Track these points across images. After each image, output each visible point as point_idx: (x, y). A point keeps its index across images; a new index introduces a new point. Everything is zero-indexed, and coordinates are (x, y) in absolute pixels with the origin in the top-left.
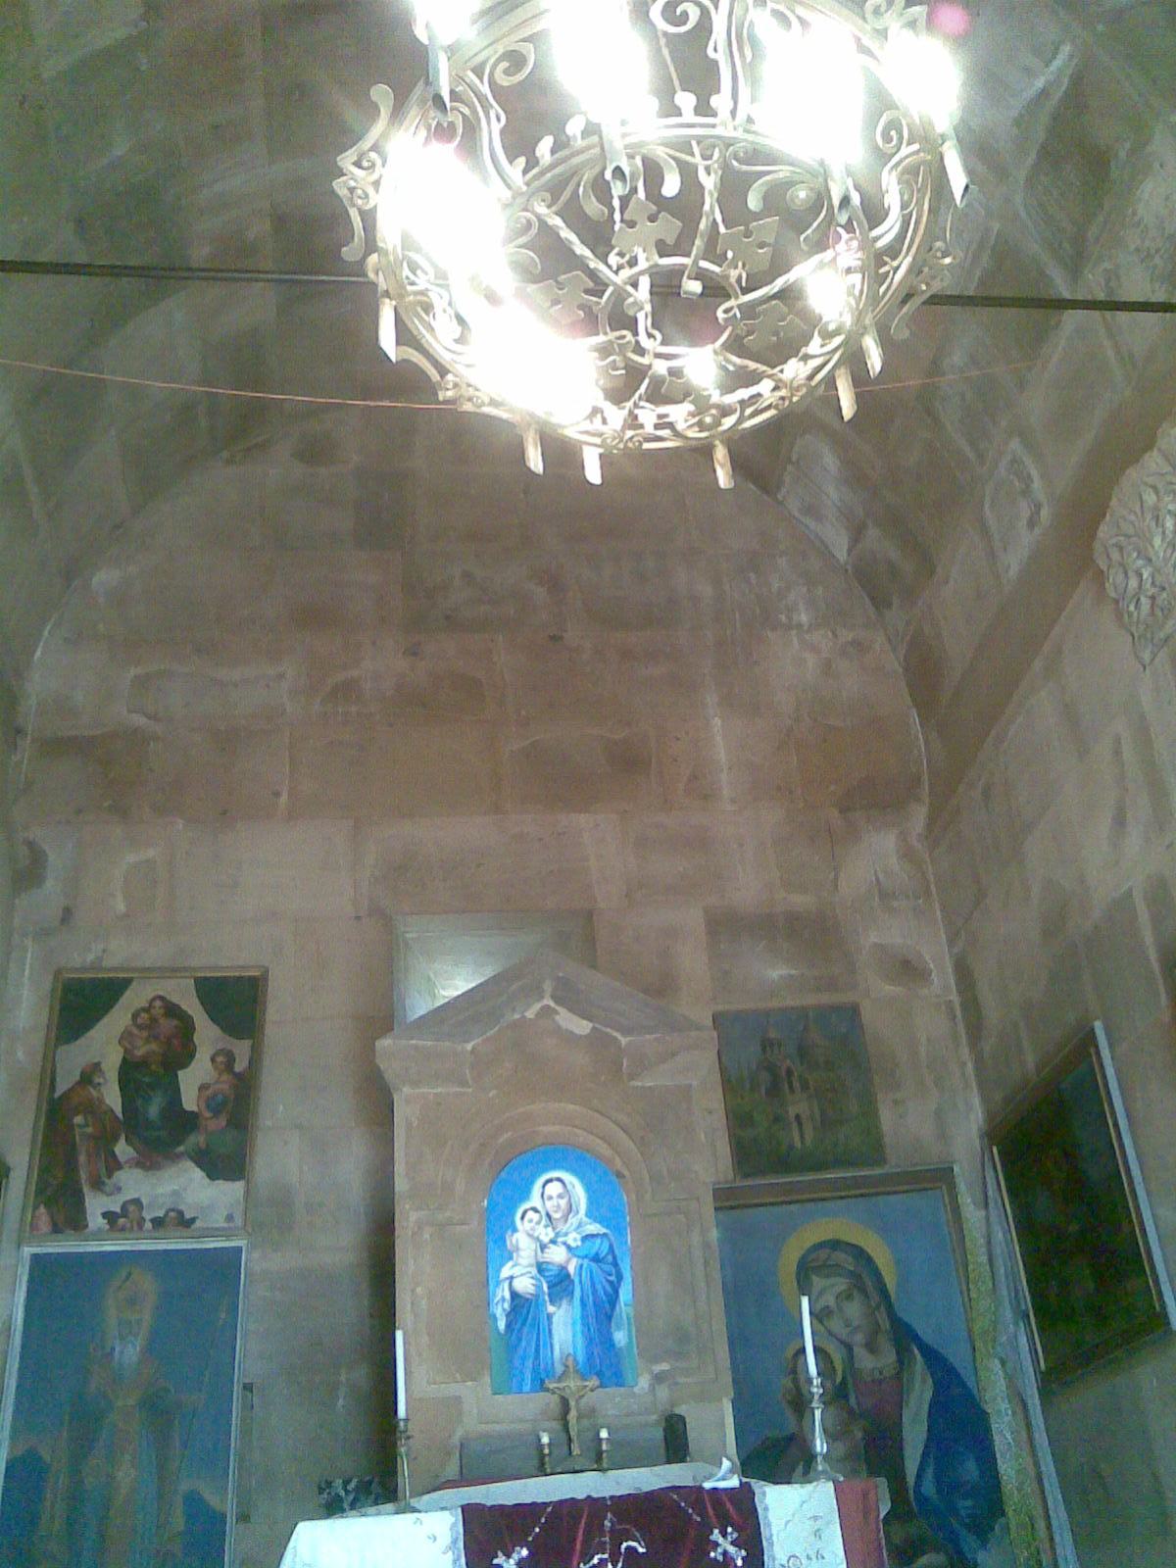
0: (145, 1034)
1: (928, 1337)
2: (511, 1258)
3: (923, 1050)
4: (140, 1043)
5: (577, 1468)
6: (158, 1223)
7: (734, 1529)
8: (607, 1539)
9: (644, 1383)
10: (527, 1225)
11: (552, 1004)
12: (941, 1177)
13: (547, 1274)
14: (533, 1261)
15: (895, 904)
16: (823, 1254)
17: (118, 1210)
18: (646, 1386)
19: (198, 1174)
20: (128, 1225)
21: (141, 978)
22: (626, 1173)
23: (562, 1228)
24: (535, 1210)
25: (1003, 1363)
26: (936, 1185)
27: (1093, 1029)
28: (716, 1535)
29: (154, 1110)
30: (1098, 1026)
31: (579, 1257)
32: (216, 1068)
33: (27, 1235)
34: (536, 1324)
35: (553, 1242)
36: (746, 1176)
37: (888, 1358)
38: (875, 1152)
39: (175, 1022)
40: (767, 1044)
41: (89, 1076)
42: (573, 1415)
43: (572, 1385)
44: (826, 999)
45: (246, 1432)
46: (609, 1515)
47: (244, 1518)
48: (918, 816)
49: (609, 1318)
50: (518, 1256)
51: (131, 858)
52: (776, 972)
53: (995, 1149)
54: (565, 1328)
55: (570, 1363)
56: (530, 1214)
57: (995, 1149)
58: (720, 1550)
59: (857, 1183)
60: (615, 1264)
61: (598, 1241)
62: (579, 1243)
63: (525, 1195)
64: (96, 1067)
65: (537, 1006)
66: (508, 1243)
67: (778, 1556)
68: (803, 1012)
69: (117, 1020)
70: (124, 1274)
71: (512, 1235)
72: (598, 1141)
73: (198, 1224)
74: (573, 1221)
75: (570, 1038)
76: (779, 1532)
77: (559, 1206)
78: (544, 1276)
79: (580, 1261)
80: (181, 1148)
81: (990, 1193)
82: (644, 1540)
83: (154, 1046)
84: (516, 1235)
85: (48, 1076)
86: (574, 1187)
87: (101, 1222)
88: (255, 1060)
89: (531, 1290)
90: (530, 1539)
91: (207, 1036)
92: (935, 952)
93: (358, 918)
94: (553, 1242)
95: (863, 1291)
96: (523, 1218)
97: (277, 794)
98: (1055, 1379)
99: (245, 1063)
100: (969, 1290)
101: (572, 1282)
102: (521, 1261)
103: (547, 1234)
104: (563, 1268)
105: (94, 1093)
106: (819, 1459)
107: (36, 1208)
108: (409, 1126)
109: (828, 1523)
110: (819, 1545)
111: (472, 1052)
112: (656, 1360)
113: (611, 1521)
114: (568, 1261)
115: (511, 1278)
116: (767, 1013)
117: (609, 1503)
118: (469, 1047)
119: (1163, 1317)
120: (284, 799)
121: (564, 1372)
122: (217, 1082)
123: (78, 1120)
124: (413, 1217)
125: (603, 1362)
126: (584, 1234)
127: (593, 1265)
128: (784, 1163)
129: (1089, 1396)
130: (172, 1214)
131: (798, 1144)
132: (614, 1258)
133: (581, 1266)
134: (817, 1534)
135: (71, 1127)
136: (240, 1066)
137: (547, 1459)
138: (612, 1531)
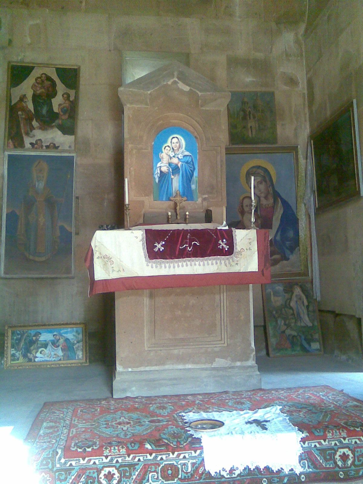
0: (40, 86)
1: (283, 196)
2: (161, 161)
3: (293, 109)
4: (38, 89)
5: (179, 222)
6: (47, 147)
7: (226, 241)
8: (188, 241)
9: (200, 200)
10: (166, 151)
11: (177, 80)
12: (294, 149)
13: (172, 166)
14: (167, 162)
15: (290, 58)
16: (254, 170)
17: (35, 143)
18: (200, 201)
19: (59, 133)
20: (38, 147)
21: (38, 66)
22: (198, 137)
23: (177, 152)
24: (169, 146)
25: (305, 205)
26: (291, 151)
27: (352, 102)
28: (220, 242)
29: (44, 111)
30: (355, 101)
31: (181, 162)
32: (64, 99)
33: (6, 148)
34: (168, 180)
35: (174, 157)
36: (233, 144)
37: (271, 201)
38: (274, 140)
39: (49, 83)
40: (243, 103)
41: (23, 98)
42: (178, 208)
43: (178, 199)
44: (264, 89)
45: (77, 207)
46: (189, 234)
47: (77, 234)
48: (302, 27)
49: (190, 181)
50: (163, 160)
51: (31, 23)
52: (249, 79)
53: (312, 141)
54: (176, 183)
55: (178, 193)
56: (167, 148)
57: (312, 141)
58: (221, 246)
59: (268, 148)
60: (193, 165)
61: (188, 157)
62: (182, 158)
63: (166, 142)
64: (24, 96)
65: (172, 80)
66: (160, 156)
67: (238, 248)
68: (256, 93)
69: (30, 81)
70: (38, 162)
71: (161, 154)
72: (189, 126)
73: (60, 148)
74: (181, 150)
75: (182, 92)
76: (239, 242)
77: (176, 145)
78: (171, 167)
79: (182, 163)
80: (54, 124)
81: (308, 154)
82: (199, 241)
83: (43, 90)
84: (162, 154)
85: (9, 98)
86: (181, 140)
87: (30, 146)
88: (77, 97)
89: (167, 171)
90: (165, 239)
91: (61, 88)
92: (301, 77)
93: (110, 51)
94: (174, 157)
95: (266, 181)
96: (165, 149)
97: (81, 2)
98: (320, 210)
99: (74, 98)
100: (298, 183)
101: (180, 169)
102: (163, 162)
103: (172, 154)
104: (177, 165)
105: (25, 105)
106: (252, 223)
107: (8, 140)
108: (129, 117)
109: (253, 241)
110: (250, 246)
111: (150, 94)
112: (204, 194)
113: (189, 236)
114: (179, 163)
115: (160, 167)
116: (244, 93)
117: (189, 231)
118: (149, 92)
119: (359, 192)
120: (84, 4)
121: (176, 195)
122: (64, 103)
123: (20, 113)
124: (130, 146)
125: (187, 193)
126: (184, 155)
127: (186, 164)
128: (245, 141)
129: (330, 215)
130: (52, 145)
131: (250, 136)
132: (193, 162)
133: (182, 165)
134: (250, 243)
135: (18, 116)
136: (72, 99)
137: (170, 219)
138: (190, 239)
